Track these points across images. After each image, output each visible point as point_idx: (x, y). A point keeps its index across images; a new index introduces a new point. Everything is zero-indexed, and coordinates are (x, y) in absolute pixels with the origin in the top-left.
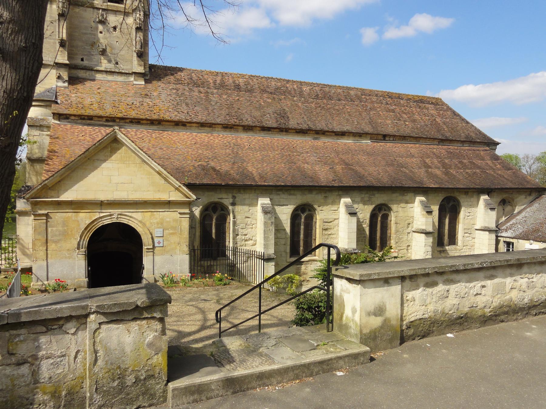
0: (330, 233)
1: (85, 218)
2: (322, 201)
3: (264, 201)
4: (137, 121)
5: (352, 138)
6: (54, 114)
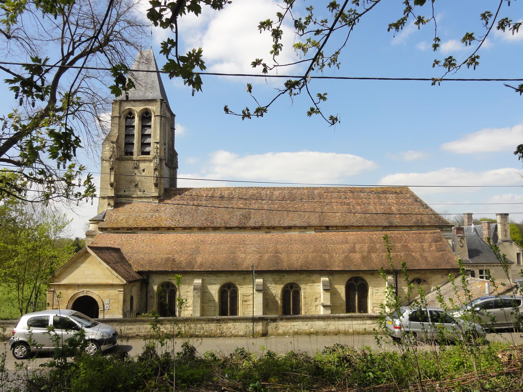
0: (248, 303)
1: (71, 293)
2: (242, 281)
3: (198, 281)
4: (145, 229)
5: (298, 230)
6: (99, 228)
